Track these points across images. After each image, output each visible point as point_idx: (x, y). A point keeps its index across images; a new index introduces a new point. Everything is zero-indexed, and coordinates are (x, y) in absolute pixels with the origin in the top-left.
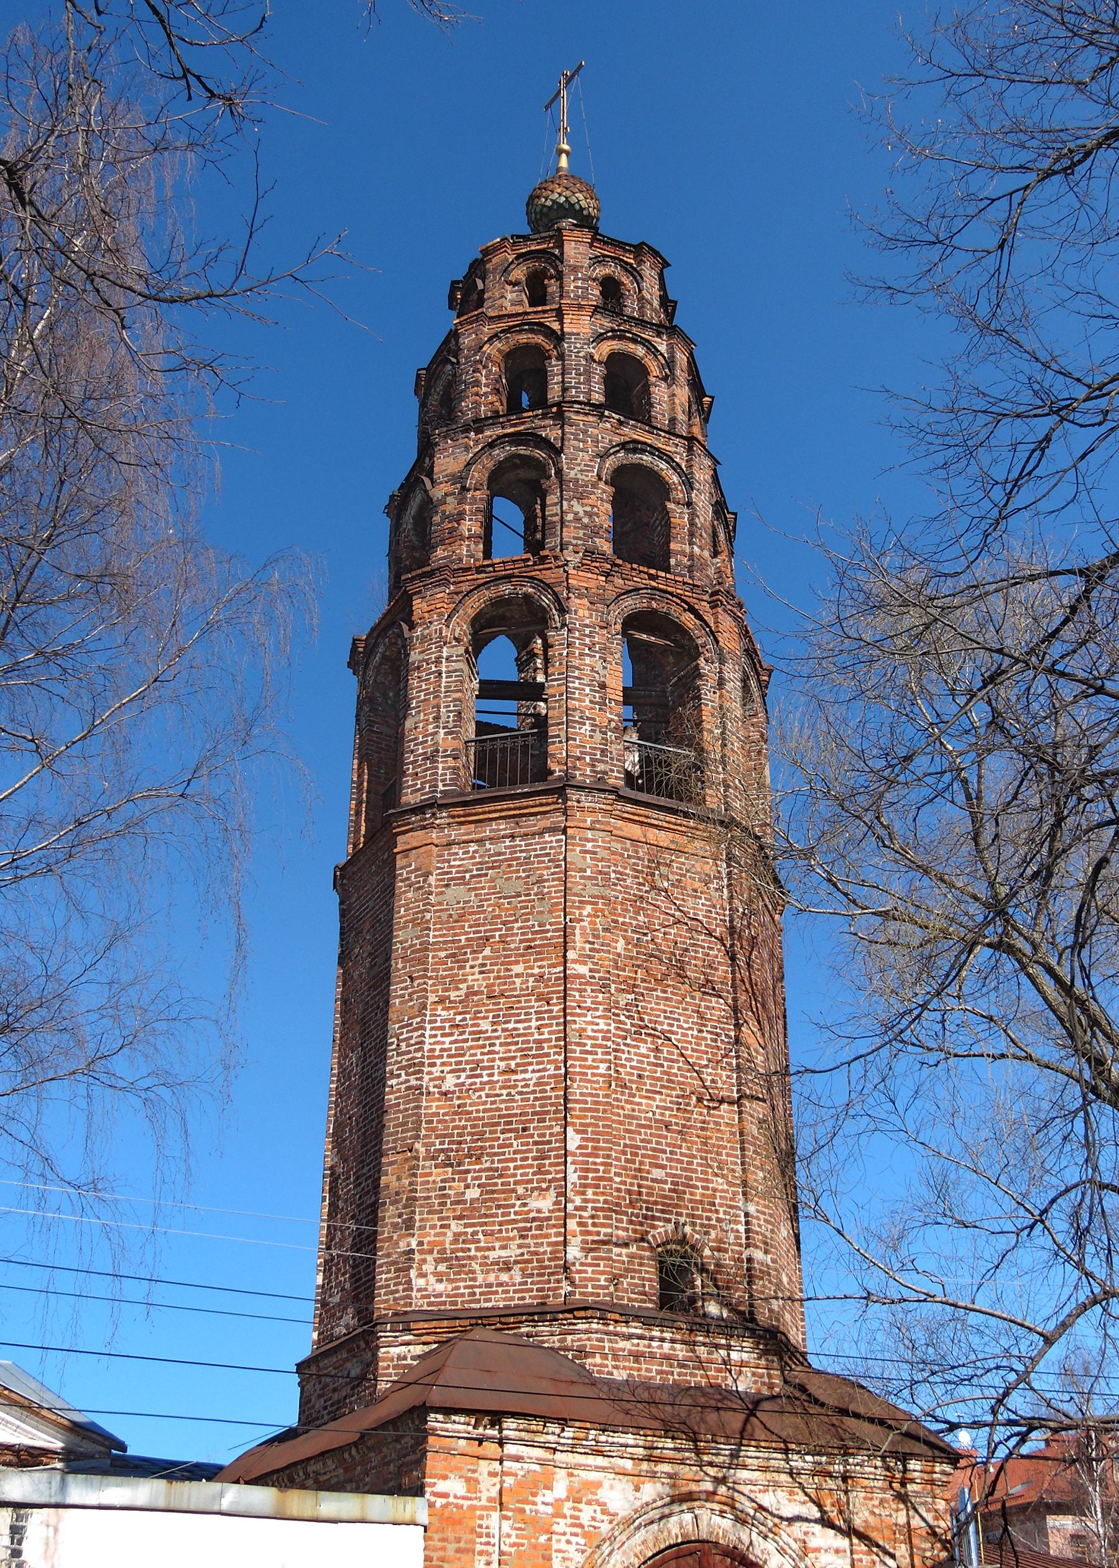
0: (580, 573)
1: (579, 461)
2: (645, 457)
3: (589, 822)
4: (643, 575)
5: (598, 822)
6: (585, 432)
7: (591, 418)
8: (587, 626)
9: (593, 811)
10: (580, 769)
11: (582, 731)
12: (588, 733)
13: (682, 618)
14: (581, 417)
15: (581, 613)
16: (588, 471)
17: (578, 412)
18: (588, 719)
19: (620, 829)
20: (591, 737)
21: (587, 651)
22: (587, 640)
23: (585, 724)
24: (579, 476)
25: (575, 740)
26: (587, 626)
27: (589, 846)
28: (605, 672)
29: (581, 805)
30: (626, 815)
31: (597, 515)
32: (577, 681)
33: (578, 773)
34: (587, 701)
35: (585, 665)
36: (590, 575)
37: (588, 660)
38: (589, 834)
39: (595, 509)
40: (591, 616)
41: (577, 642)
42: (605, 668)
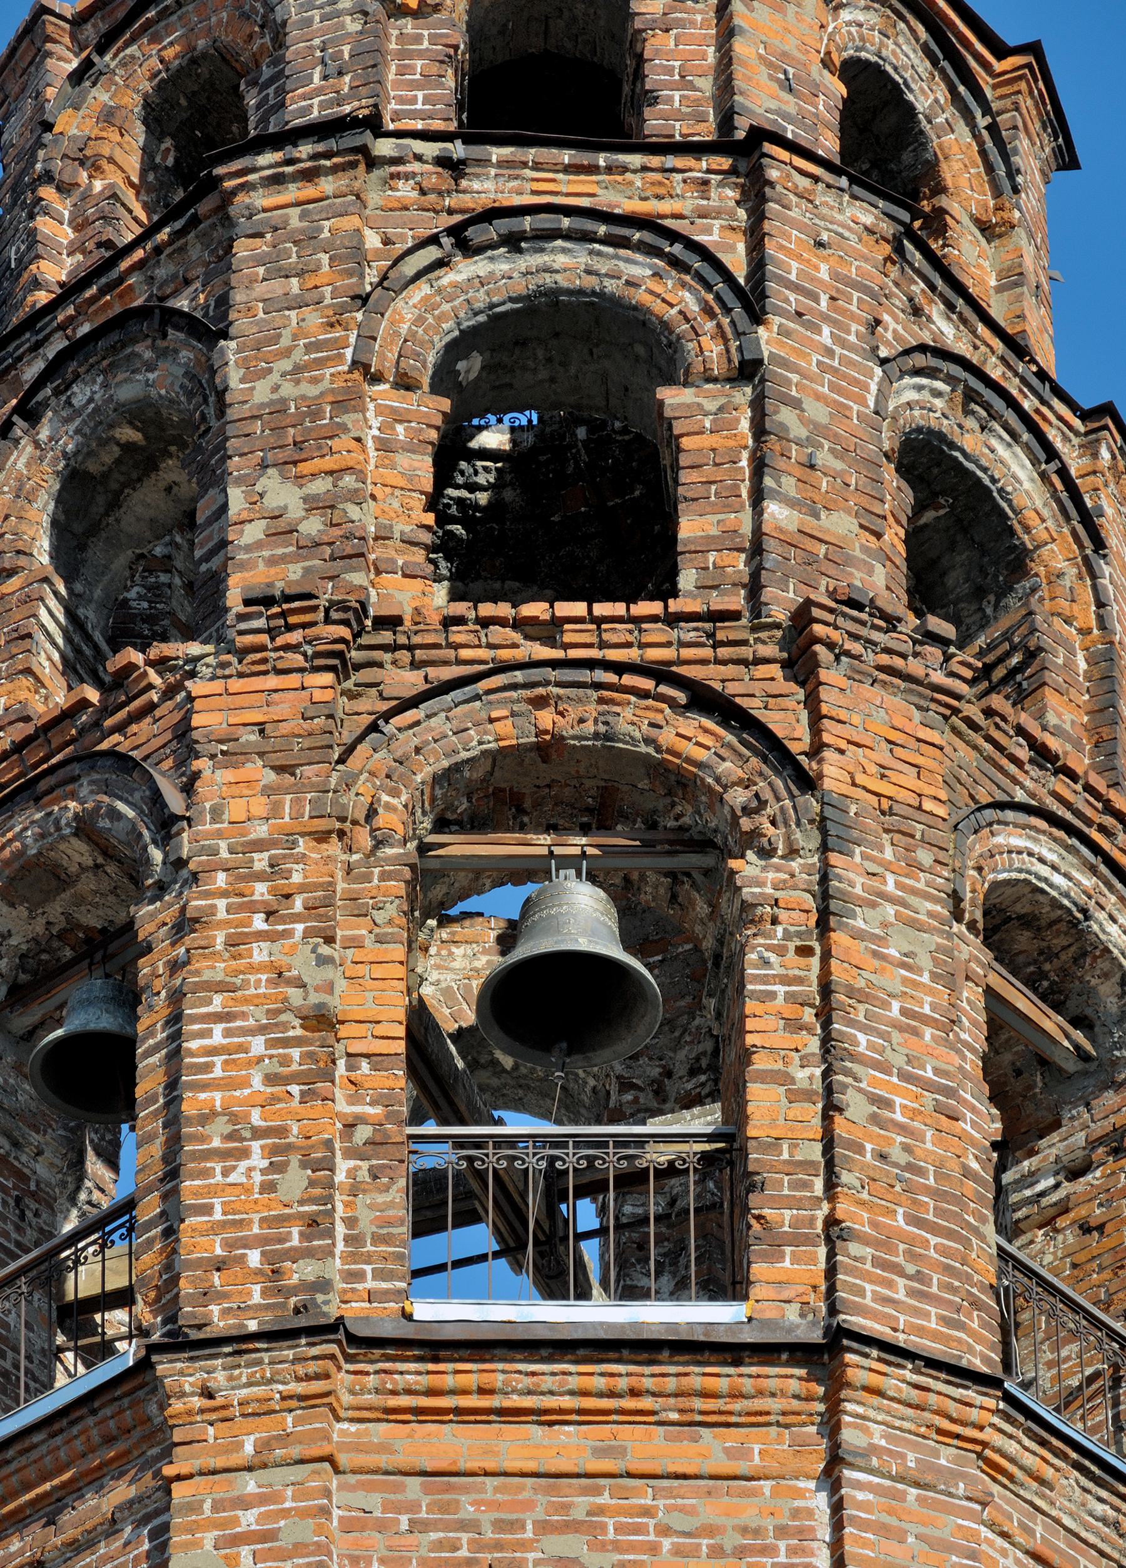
0: (236, 685)
1: (285, 341)
2: (561, 260)
3: (249, 1448)
4: (497, 633)
5: (285, 1438)
6: (307, 239)
7: (327, 185)
8: (259, 846)
9: (262, 1411)
10: (223, 1296)
11: (233, 1178)
12: (258, 1178)
13: (667, 737)
14: (293, 192)
15: (236, 810)
16: (320, 363)
17: (277, 180)
18: (258, 1133)
19: (384, 1448)
20: (269, 1187)
21: (259, 922)
22: (261, 890)
23: (245, 1154)
24: (288, 390)
25: (208, 1210)
26: (259, 846)
27: (249, 1519)
28: (329, 972)
29: (219, 1401)
30: (405, 1401)
31: (356, 498)
32: (218, 1029)
33: (215, 1309)
34: (257, 1082)
35: (252, 969)
36: (272, 681)
37: (260, 953)
38: (250, 1484)
39: (348, 480)
40: (275, 811)
41: (221, 904)
42: (323, 961)
